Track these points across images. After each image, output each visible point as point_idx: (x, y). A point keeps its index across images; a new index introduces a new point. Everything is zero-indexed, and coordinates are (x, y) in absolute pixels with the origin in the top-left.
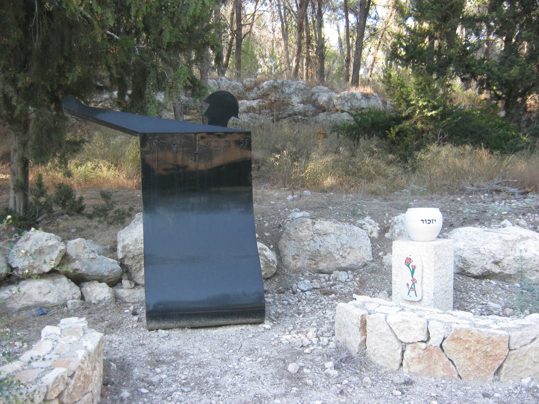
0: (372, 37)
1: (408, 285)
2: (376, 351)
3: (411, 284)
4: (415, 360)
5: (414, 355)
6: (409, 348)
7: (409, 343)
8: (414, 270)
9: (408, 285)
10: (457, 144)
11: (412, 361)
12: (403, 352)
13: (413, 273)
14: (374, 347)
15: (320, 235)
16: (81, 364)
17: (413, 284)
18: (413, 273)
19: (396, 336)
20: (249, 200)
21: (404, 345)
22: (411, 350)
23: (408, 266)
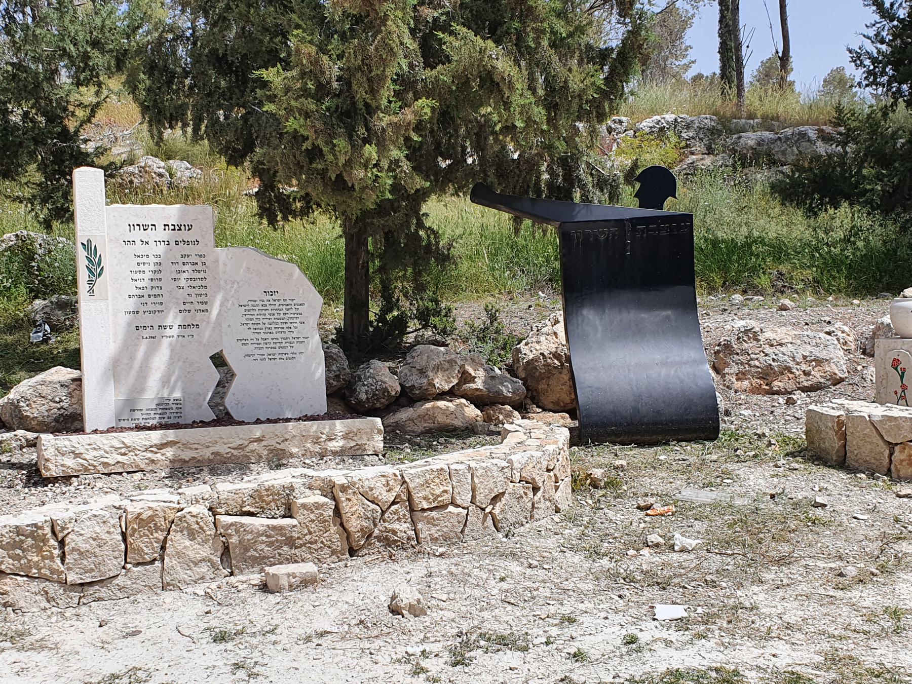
0: (823, 42)
1: (896, 393)
2: (859, 456)
3: (899, 391)
4: (904, 463)
5: (903, 456)
6: (897, 448)
7: (897, 444)
8: (903, 373)
9: (896, 393)
10: (412, 407)
11: (900, 464)
12: (891, 454)
13: (902, 377)
14: (856, 452)
15: (772, 345)
16: (733, 340)
17: (903, 391)
18: (902, 377)
19: (882, 437)
20: (691, 306)
21: (891, 446)
22: (901, 452)
23: (896, 369)
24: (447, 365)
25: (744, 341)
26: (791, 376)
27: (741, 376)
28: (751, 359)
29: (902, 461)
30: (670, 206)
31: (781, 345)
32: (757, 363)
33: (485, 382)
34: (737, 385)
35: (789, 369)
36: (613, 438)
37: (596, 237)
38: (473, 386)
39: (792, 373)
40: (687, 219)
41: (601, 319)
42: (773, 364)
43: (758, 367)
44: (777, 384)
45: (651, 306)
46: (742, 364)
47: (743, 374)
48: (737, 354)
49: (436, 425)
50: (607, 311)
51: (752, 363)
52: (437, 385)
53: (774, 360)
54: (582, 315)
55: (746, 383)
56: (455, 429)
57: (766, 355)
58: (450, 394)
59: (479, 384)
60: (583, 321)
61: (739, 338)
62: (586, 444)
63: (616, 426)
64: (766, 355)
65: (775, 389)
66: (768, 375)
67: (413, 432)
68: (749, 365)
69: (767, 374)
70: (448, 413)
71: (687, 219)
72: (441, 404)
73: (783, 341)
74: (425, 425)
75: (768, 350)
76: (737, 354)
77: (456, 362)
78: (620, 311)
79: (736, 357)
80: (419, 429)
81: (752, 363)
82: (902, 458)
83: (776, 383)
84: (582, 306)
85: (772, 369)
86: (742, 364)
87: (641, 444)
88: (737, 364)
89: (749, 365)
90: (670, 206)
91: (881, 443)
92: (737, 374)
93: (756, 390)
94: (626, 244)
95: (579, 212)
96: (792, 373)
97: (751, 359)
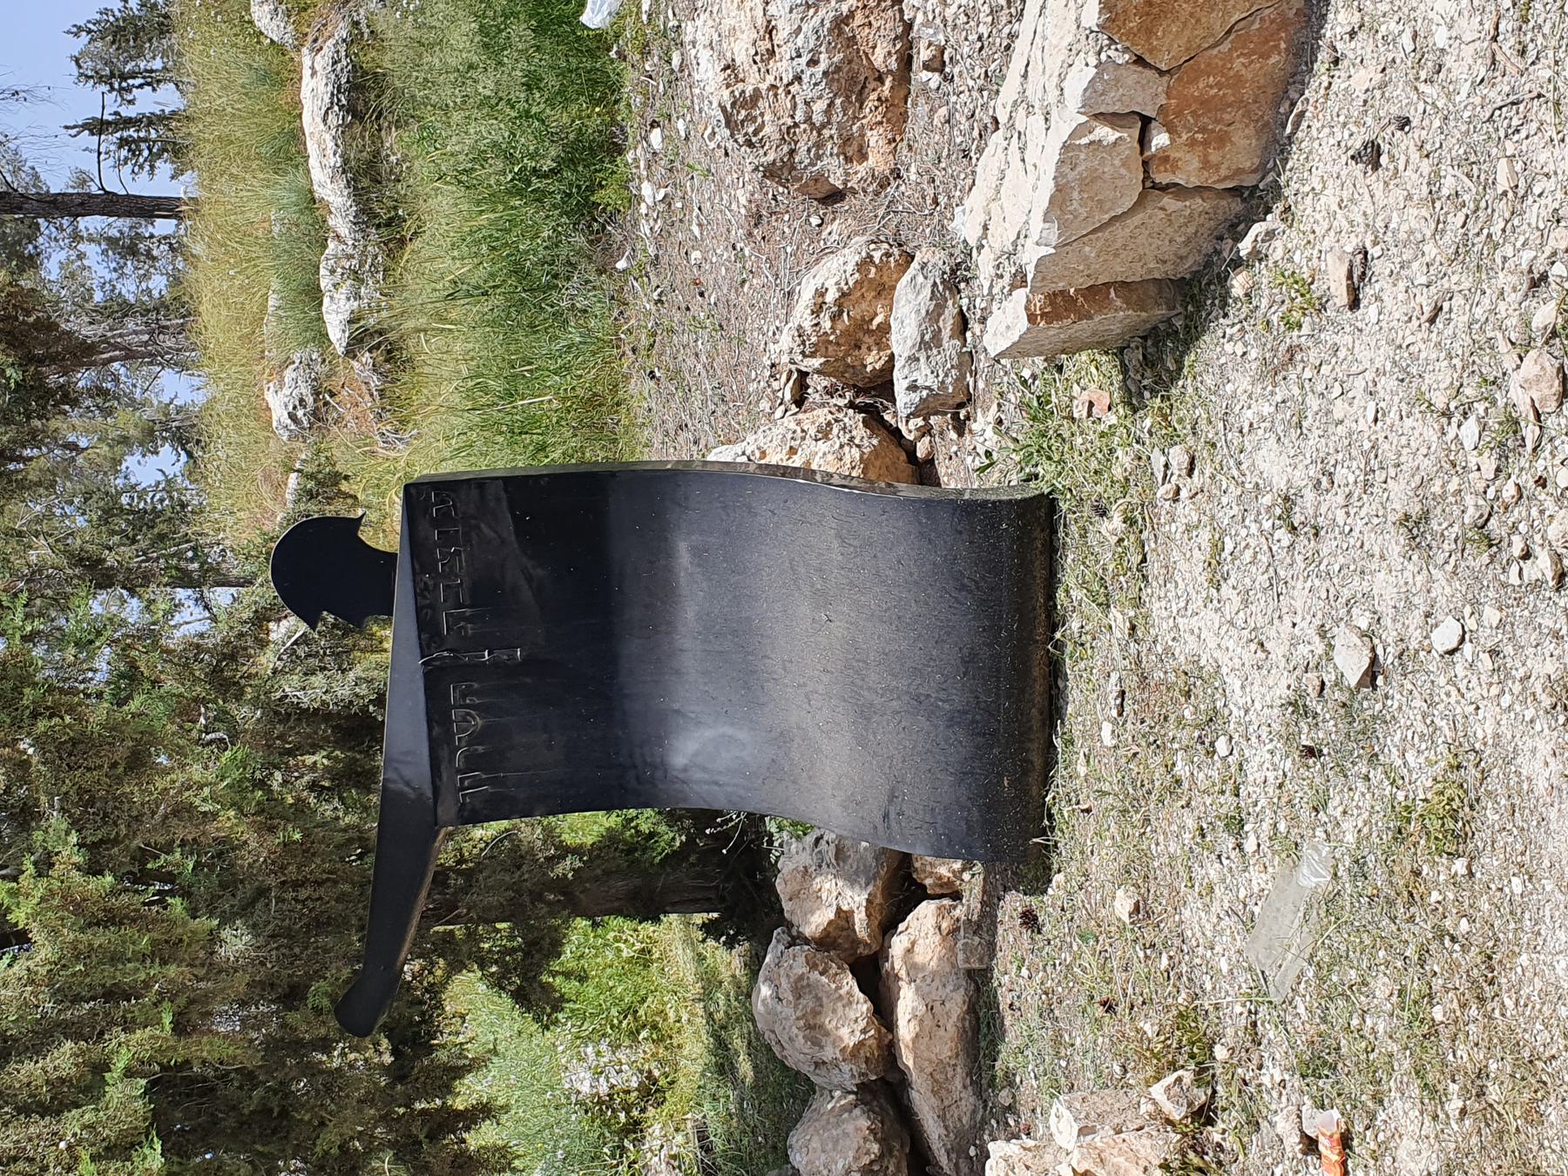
11: (1217, 167)
15: (771, 53)
24: (808, 1002)
25: (755, 133)
26: (859, 19)
27: (854, 150)
28: (808, 120)
29: (1206, 164)
30: (385, 529)
31: (770, 31)
32: (819, 106)
33: (852, 881)
34: (877, 160)
35: (841, 22)
36: (1033, 779)
37: (475, 739)
38: (860, 919)
39: (851, 14)
40: (419, 496)
41: (698, 724)
42: (822, 66)
43: (831, 105)
44: (882, 56)
45: (663, 591)
46: (819, 145)
47: (847, 141)
48: (792, 152)
49: (960, 1062)
50: (676, 706)
51: (818, 118)
52: (858, 1037)
53: (813, 62)
54: (685, 770)
55: (875, 139)
56: (972, 1008)
57: (798, 78)
58: (874, 978)
59: (856, 900)
60: (704, 769)
61: (750, 144)
62: (1048, 849)
63: (1000, 776)
64: (798, 78)
65: (894, 66)
66: (852, 79)
67: (974, 1112)
68: (823, 126)
69: (851, 82)
70: (928, 1022)
71: (419, 496)
72: (906, 1030)
73: (761, 21)
74: (958, 1083)
75: (783, 68)
76: (792, 152)
77: (801, 977)
78: (678, 672)
79: (802, 156)
80: (968, 1101)
81: (818, 118)
82: (1196, 164)
83: (878, 58)
84: (664, 766)
85: (838, 69)
86: (819, 145)
87: (1053, 710)
88: (819, 157)
89: (823, 126)
90: (385, 529)
91: (1137, 219)
92: (848, 160)
93: (896, 116)
94: (495, 664)
95: (408, 784)
96: (851, 14)
97: (808, 120)
